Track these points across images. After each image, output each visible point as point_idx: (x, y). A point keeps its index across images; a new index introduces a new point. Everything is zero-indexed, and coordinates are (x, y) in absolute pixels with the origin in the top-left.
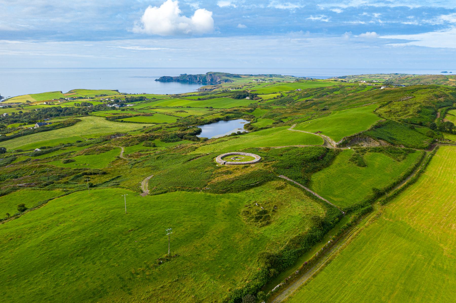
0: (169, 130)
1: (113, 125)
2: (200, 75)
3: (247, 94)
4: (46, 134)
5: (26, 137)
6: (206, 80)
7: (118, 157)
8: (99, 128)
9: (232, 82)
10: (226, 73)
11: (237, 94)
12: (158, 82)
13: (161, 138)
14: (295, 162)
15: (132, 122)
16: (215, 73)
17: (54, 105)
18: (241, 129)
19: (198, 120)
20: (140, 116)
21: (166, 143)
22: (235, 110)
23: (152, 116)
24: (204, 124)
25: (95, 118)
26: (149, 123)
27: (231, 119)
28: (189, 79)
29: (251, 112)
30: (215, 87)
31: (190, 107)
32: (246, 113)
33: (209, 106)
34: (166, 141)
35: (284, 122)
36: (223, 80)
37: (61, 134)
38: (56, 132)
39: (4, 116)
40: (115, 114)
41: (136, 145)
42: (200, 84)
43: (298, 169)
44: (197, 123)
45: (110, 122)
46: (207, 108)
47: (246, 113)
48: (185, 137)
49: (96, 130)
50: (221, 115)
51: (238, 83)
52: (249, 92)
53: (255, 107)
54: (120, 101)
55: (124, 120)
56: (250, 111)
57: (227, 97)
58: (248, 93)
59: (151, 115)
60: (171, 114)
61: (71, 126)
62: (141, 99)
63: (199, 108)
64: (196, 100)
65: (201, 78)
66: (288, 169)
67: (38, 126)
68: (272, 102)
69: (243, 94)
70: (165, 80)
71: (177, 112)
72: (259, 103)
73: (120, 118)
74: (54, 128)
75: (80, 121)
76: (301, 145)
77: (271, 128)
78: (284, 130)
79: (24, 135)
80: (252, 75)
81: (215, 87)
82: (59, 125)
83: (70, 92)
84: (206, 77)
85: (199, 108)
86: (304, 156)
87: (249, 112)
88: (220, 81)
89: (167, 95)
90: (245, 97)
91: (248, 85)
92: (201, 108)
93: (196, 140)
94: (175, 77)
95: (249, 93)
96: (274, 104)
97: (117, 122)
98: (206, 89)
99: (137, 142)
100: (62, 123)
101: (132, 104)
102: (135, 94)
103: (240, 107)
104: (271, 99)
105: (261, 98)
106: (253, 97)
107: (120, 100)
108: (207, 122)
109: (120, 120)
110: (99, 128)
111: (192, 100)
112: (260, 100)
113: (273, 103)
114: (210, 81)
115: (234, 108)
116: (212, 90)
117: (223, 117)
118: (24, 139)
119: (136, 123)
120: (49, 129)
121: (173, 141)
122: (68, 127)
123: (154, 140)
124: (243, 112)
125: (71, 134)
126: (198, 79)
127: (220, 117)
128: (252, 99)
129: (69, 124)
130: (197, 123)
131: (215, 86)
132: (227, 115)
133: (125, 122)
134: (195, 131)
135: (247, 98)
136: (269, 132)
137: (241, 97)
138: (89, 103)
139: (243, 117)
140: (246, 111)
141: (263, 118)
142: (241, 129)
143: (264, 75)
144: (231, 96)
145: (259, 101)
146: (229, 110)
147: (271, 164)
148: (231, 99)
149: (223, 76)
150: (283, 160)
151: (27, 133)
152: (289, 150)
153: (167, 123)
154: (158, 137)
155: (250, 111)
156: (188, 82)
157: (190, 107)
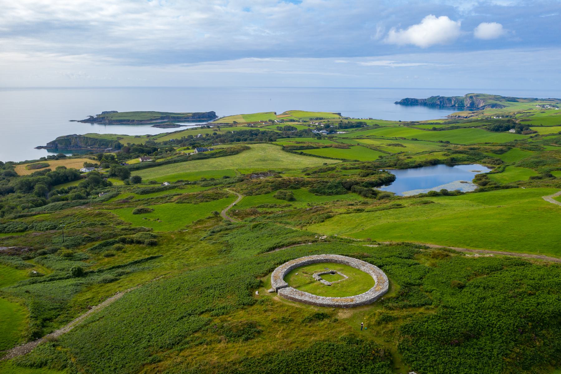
0: (344, 172)
1: (287, 157)
2: (456, 97)
3: (512, 125)
4: (199, 164)
5: (176, 164)
6: (463, 104)
7: (217, 214)
8: (267, 160)
9: (502, 108)
10: (495, 96)
11: (495, 125)
12: (399, 106)
13: (311, 187)
14: (494, 320)
15: (314, 156)
16: (477, 96)
17: (257, 127)
18: (466, 182)
19: (398, 160)
20: (331, 148)
21: (316, 195)
22: (471, 149)
23: (348, 148)
24: (407, 168)
25: (268, 146)
26: (337, 159)
27: (460, 163)
28: (441, 102)
29: (500, 154)
30: (472, 114)
31: (416, 140)
32: (490, 154)
33: (444, 140)
34: (317, 192)
35: (555, 178)
36: (489, 105)
37: (215, 165)
38: (212, 161)
39: (198, 137)
40: (299, 143)
41: (264, 195)
42: (454, 109)
43: (495, 352)
44: (395, 165)
45: (286, 153)
46: (442, 142)
47: (490, 154)
48: (355, 188)
49: (261, 163)
50: (444, 155)
51: (511, 109)
52: (517, 122)
53: (511, 146)
54: (332, 126)
55: (304, 151)
56: (499, 152)
57: (478, 128)
58: (515, 124)
59: (348, 147)
60: (378, 148)
61: (234, 154)
62: (360, 125)
63: (429, 141)
64: (430, 130)
65: (456, 101)
66: (458, 344)
67: (197, 152)
68: (553, 139)
69: (506, 124)
70: (408, 103)
71: (390, 145)
72: (530, 140)
73: (302, 148)
74: (213, 156)
75: (248, 148)
76: (544, 255)
77: (518, 187)
78: (531, 200)
79: (175, 162)
80: (537, 99)
81: (472, 114)
82: (220, 152)
83: (285, 114)
84: (464, 100)
85: (429, 141)
86: (532, 300)
87: (497, 154)
88: (484, 106)
89: (400, 121)
90: (508, 129)
91: (524, 113)
92: (432, 142)
93: (370, 195)
94: (421, 100)
95: (517, 124)
96: (556, 143)
97: (294, 154)
98: (459, 117)
99: (269, 189)
100: (225, 150)
101: (345, 131)
102: (358, 119)
103: (486, 143)
104: (553, 134)
105: (536, 132)
106: (522, 130)
107: (333, 125)
108: (414, 165)
109: (299, 151)
110: (267, 160)
111: (425, 129)
112: (533, 135)
113: (555, 141)
114: (469, 105)
115: (474, 144)
116: (468, 117)
117: (445, 158)
118: (173, 167)
119: (320, 157)
120: (206, 156)
121: (330, 194)
122: (230, 156)
123: (300, 188)
124: (487, 152)
125: (226, 166)
126: (453, 102)
127: (441, 158)
128: (519, 133)
129: (233, 152)
130: (395, 165)
131: (473, 113)
132: (454, 156)
133: (305, 154)
134: (380, 179)
135: (512, 131)
136: (504, 197)
137: (500, 129)
138: (292, 128)
139: (482, 161)
140: (492, 151)
141: (517, 166)
142: (466, 182)
143: (557, 99)
144: (486, 127)
145: (531, 137)
146: (461, 148)
147: (405, 318)
148: (485, 131)
149: (490, 99)
150: (454, 308)
151: (178, 161)
152: (497, 270)
153: (358, 161)
154: (307, 184)
155: (499, 152)
156: (439, 107)
157: (416, 139)
